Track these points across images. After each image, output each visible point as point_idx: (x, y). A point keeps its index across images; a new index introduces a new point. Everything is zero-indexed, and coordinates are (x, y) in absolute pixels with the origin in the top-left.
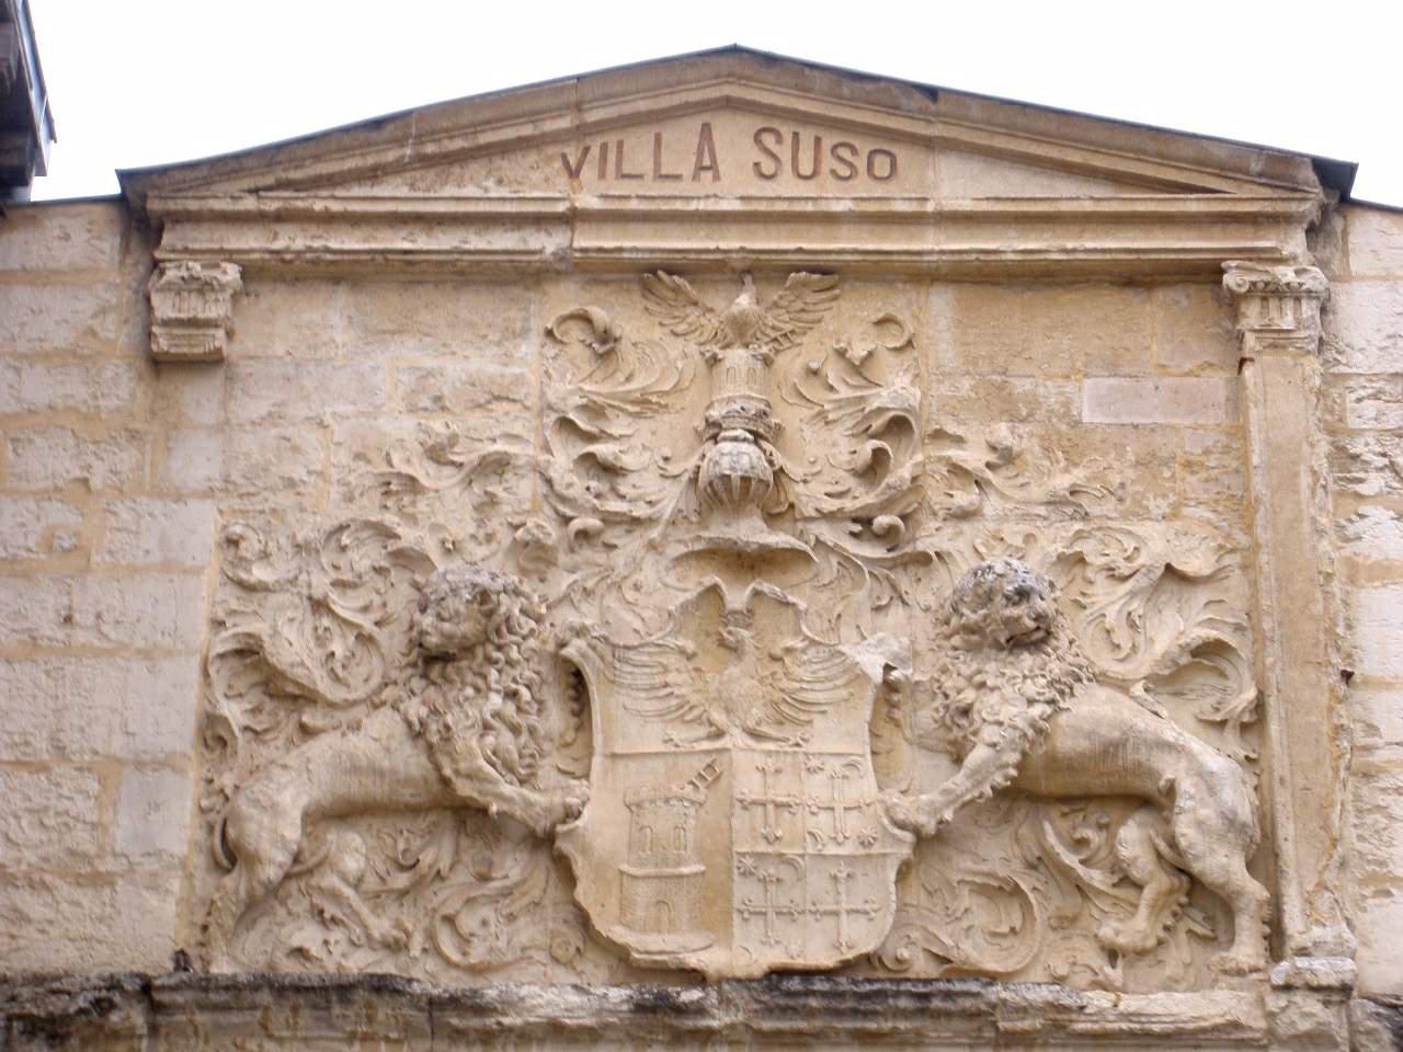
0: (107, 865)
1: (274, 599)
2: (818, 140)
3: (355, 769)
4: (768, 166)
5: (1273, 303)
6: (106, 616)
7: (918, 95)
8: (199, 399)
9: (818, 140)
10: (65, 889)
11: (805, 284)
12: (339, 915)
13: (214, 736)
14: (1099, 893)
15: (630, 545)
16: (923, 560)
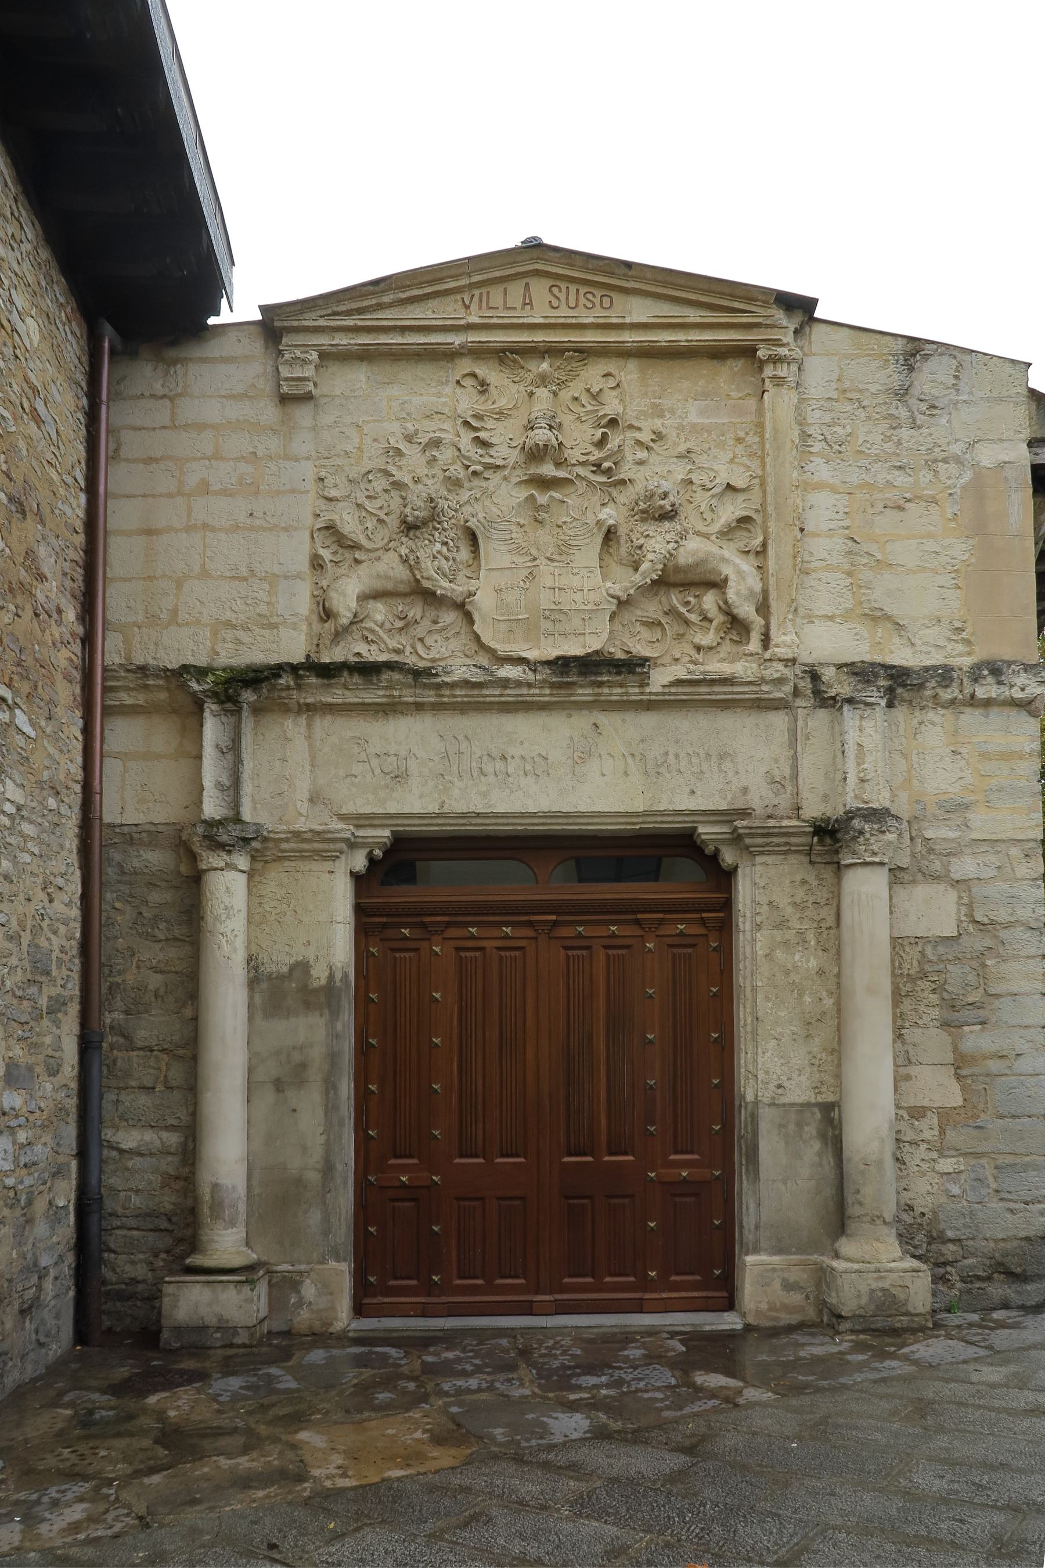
0: (275, 620)
1: (341, 504)
2: (578, 290)
3: (379, 576)
4: (555, 303)
5: (778, 365)
7: (623, 266)
8: (303, 414)
9: (578, 290)
10: (257, 630)
11: (572, 358)
13: (317, 564)
15: (496, 478)
16: (623, 482)
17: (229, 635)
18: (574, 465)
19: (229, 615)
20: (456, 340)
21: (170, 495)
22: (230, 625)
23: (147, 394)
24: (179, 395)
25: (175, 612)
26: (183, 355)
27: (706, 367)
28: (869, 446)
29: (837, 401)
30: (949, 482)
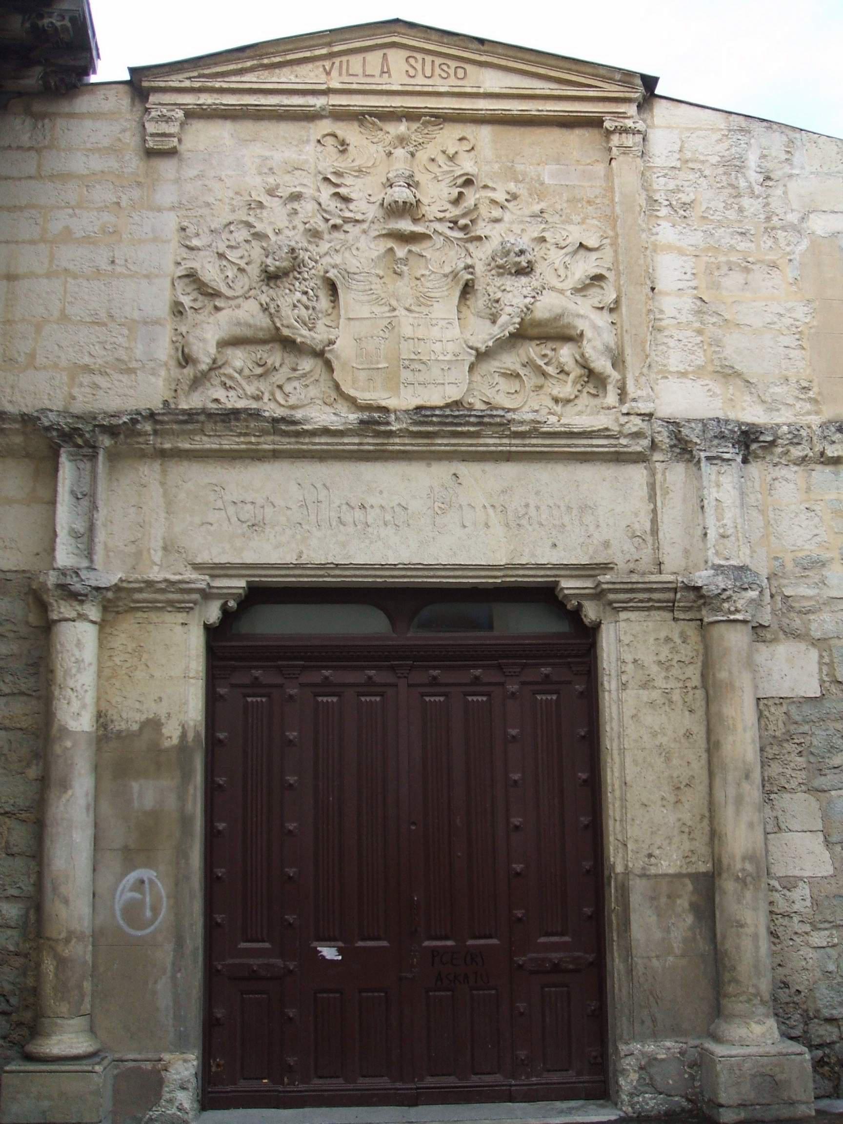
0: (133, 365)
1: (202, 253)
2: (433, 61)
3: (239, 324)
6: (129, 261)
10: (116, 376)
11: (429, 122)
12: (233, 385)
13: (178, 310)
14: (551, 376)
16: (479, 238)
17: (86, 379)
18: (431, 221)
19: (87, 360)
20: (319, 102)
21: (32, 242)
22: (87, 369)
23: (14, 145)
24: (45, 147)
25: (32, 356)
26: (52, 109)
27: (557, 134)
28: (711, 212)
29: (679, 169)
30: (788, 249)
